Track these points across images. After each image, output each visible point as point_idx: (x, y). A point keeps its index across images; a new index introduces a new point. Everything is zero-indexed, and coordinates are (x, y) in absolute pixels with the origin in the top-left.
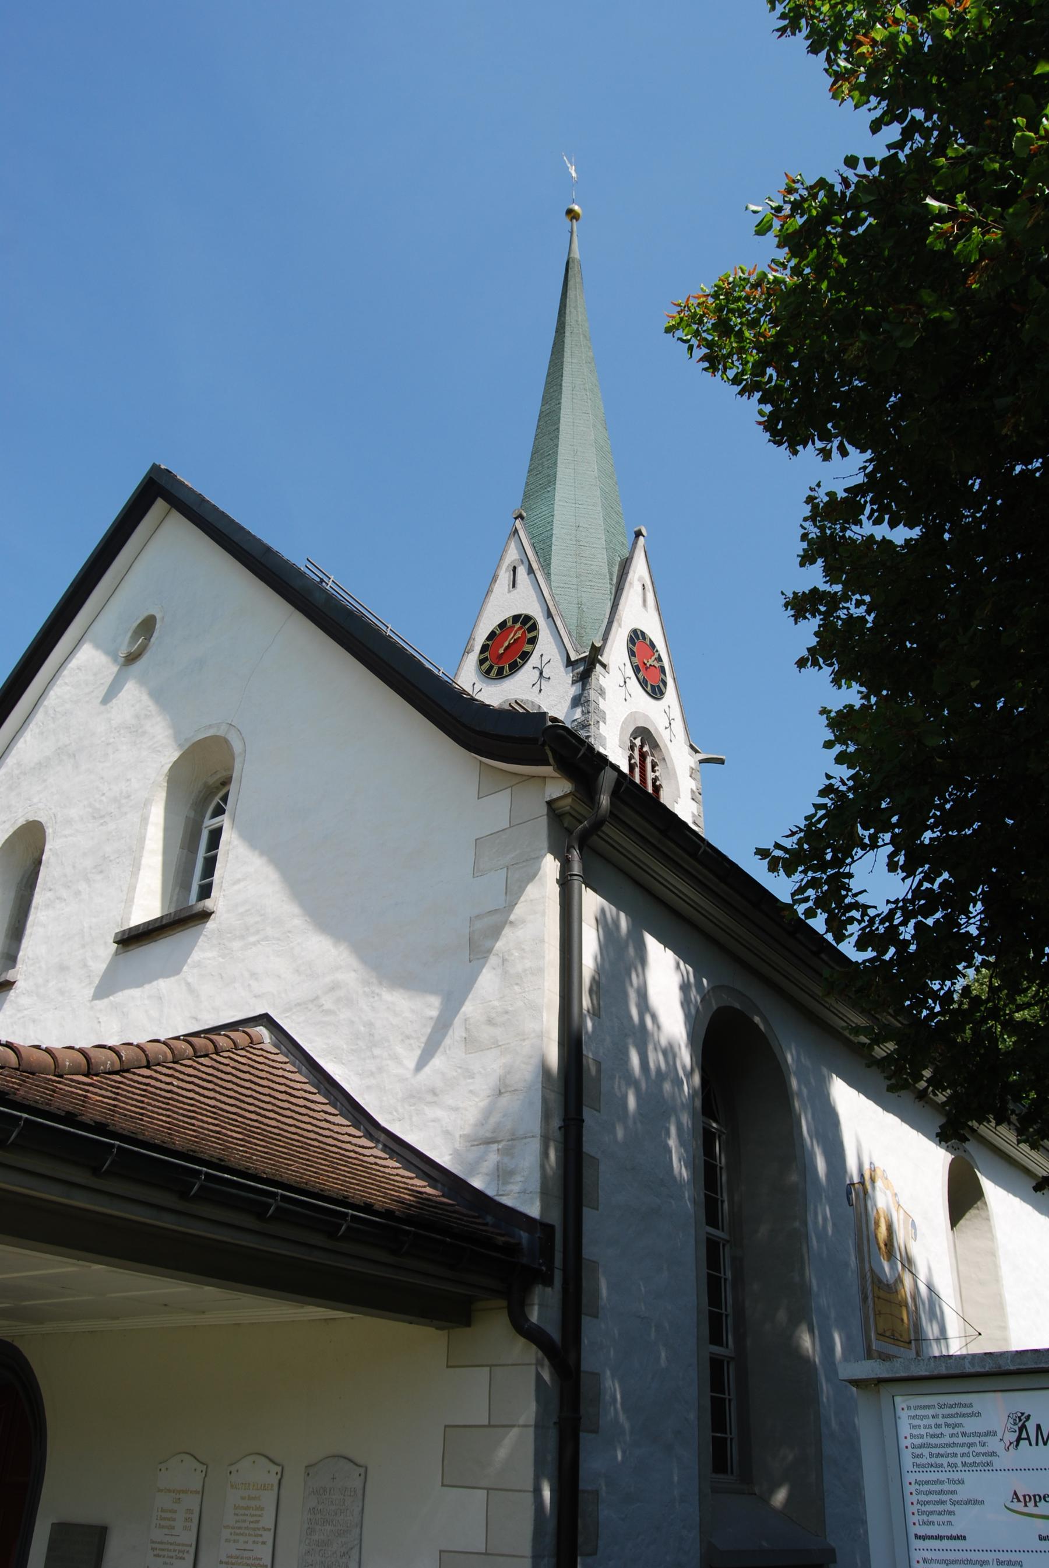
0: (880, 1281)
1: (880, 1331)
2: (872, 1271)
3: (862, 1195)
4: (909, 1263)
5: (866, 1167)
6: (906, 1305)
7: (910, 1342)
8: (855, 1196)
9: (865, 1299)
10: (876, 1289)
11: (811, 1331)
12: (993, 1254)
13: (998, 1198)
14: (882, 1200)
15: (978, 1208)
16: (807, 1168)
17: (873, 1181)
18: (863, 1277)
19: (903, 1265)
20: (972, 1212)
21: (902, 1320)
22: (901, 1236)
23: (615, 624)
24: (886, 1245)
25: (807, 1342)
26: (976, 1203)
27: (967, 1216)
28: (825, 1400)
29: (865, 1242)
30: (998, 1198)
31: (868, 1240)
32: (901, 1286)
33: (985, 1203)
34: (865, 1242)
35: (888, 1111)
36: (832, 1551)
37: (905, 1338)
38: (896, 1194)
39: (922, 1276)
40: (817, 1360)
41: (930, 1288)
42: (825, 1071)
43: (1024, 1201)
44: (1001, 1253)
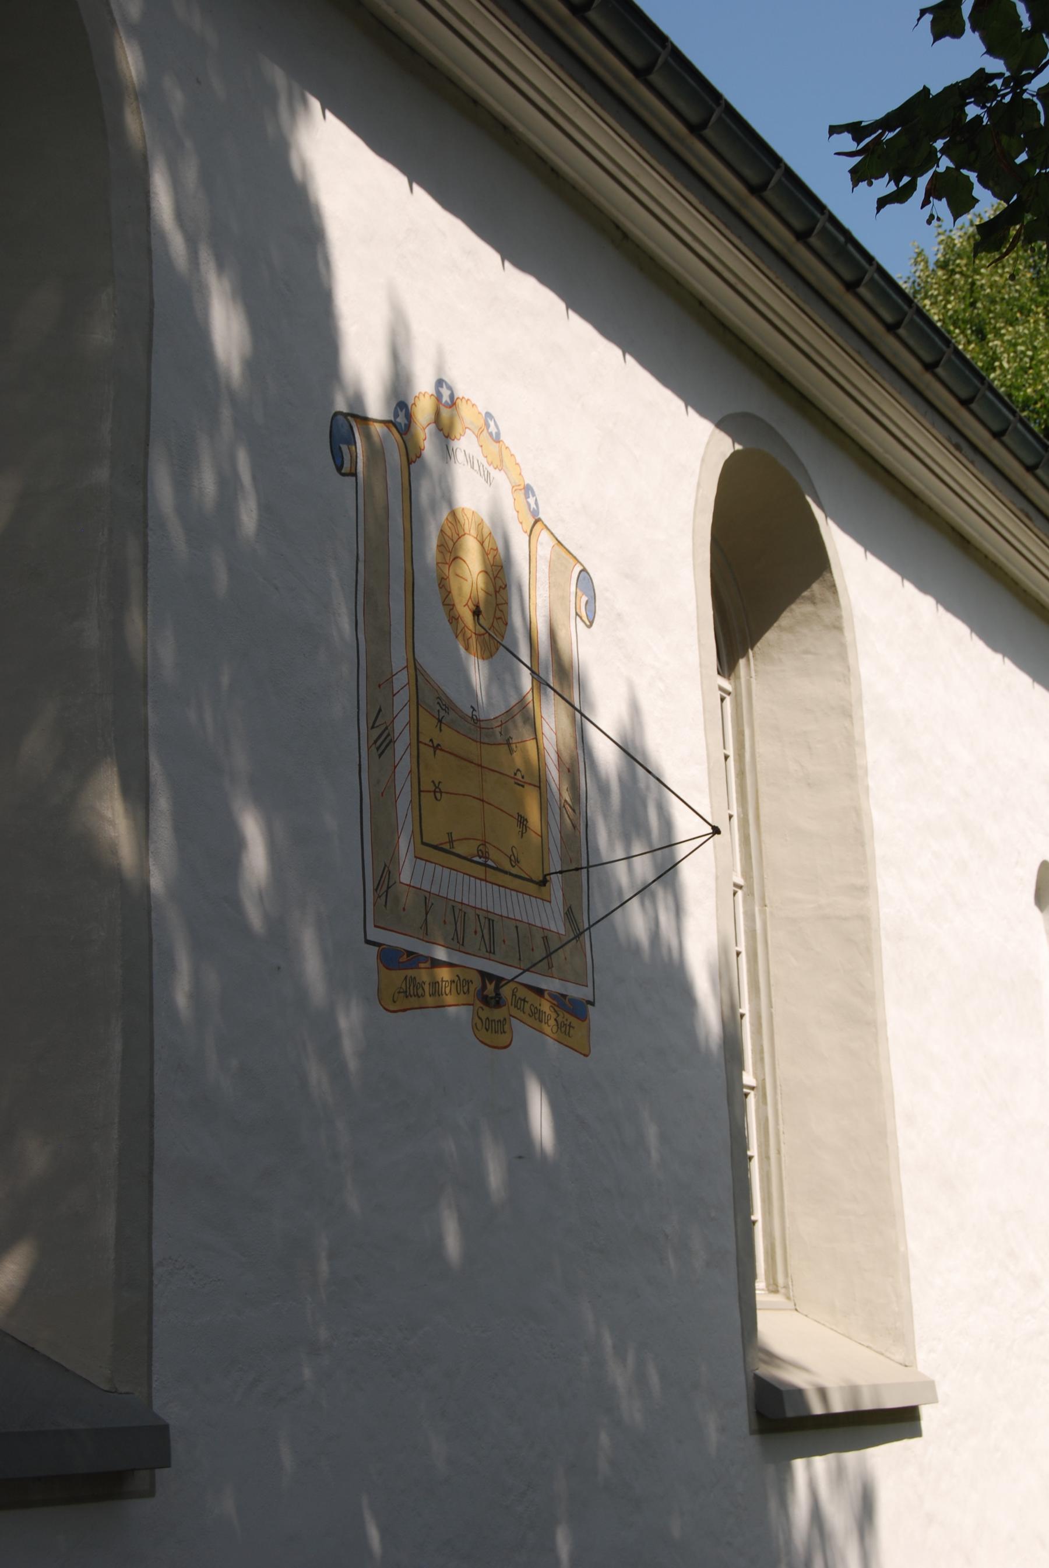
0: (446, 705)
1: (437, 837)
2: (417, 670)
3: (395, 457)
4: (561, 676)
5: (423, 385)
6: (540, 784)
7: (544, 882)
8: (376, 468)
9: (383, 743)
10: (428, 724)
11: (138, 795)
12: (846, 711)
13: (875, 598)
14: (474, 490)
15: (812, 600)
16: (160, 318)
17: (445, 432)
18: (377, 680)
19: (539, 681)
20: (798, 610)
21: (522, 821)
22: (540, 600)
23: (151, 814)
24: (477, 613)
25: (113, 818)
26: (807, 585)
27: (785, 619)
28: (182, 1000)
29: (397, 588)
30: (875, 598)
31: (411, 587)
32: (526, 733)
33: (833, 587)
34: (397, 588)
35: (522, 265)
36: (161, 1431)
37: (530, 867)
38: (528, 490)
39: (608, 714)
40: (157, 882)
41: (631, 754)
42: (279, 78)
43: (948, 608)
44: (867, 710)
